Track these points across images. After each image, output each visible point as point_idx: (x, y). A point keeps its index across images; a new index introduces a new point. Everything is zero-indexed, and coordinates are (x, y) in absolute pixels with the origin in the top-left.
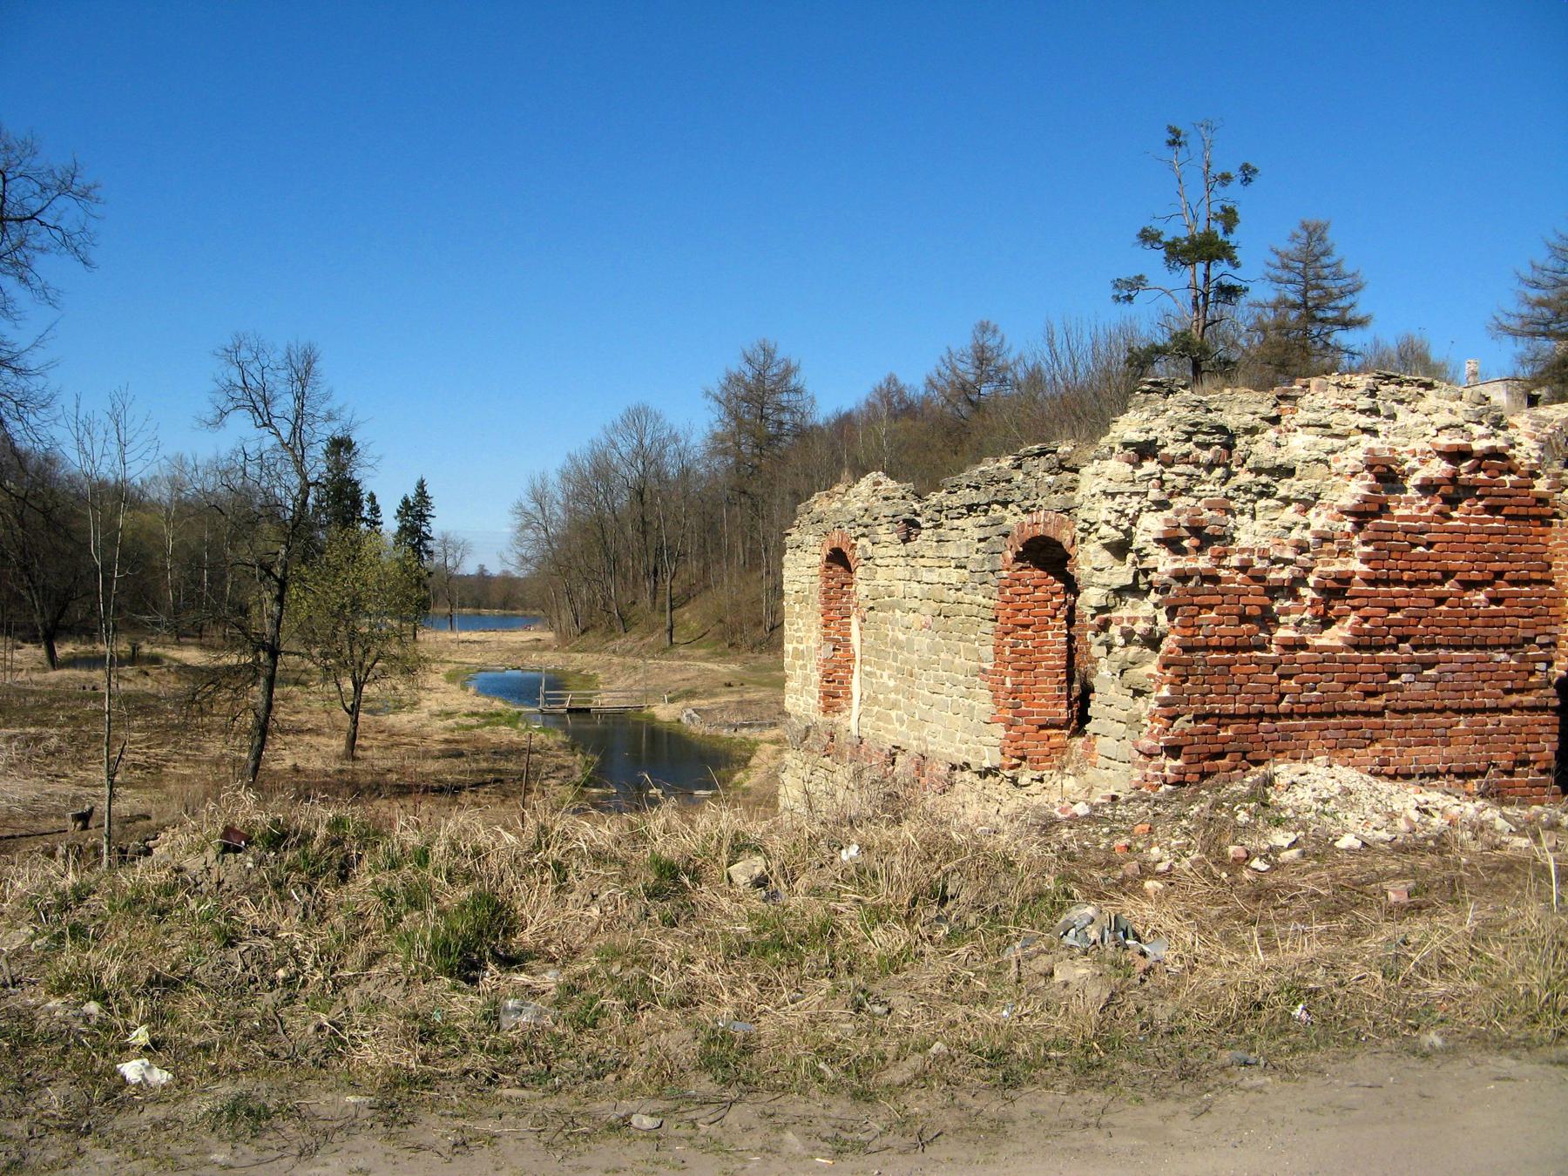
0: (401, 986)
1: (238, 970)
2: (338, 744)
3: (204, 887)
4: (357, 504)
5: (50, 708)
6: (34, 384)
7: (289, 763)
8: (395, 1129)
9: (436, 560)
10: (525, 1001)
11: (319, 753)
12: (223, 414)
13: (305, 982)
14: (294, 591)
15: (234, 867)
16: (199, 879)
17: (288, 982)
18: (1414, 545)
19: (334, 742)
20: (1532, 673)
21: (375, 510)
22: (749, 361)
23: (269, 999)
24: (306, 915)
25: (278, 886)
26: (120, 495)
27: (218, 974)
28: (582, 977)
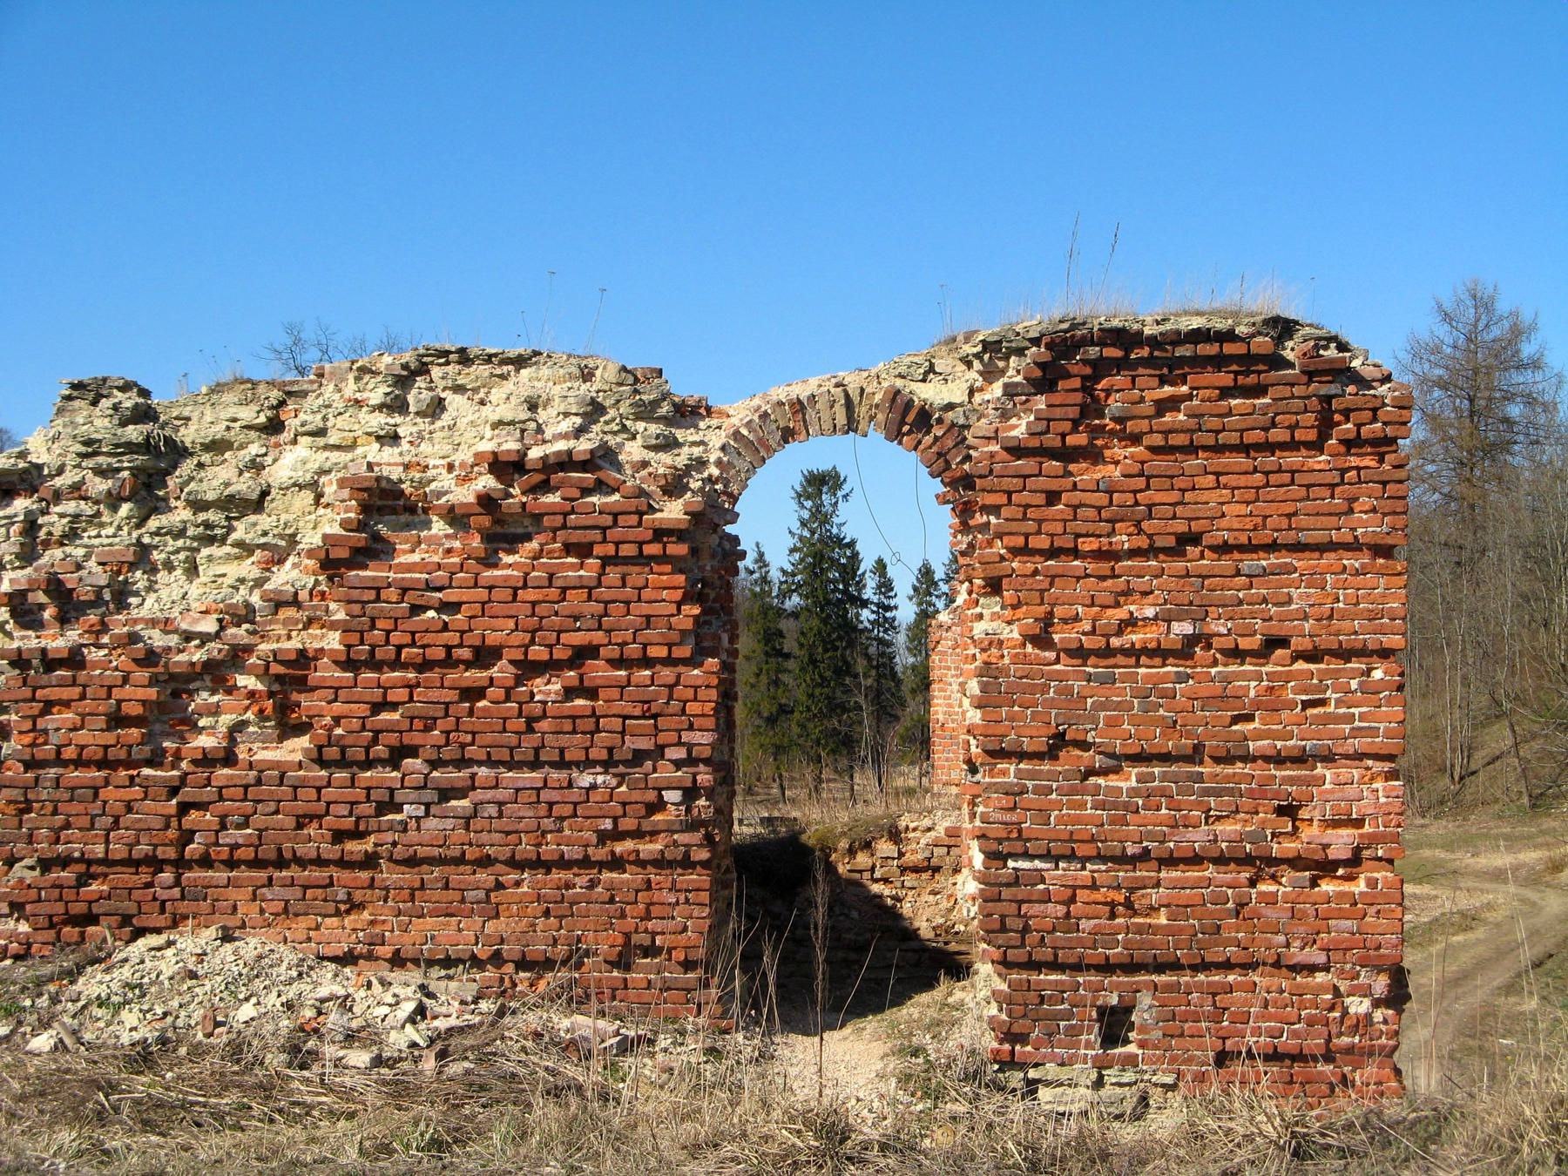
4: (850, 569)
18: (416, 609)
20: (660, 805)
21: (886, 586)
22: (1447, 318)
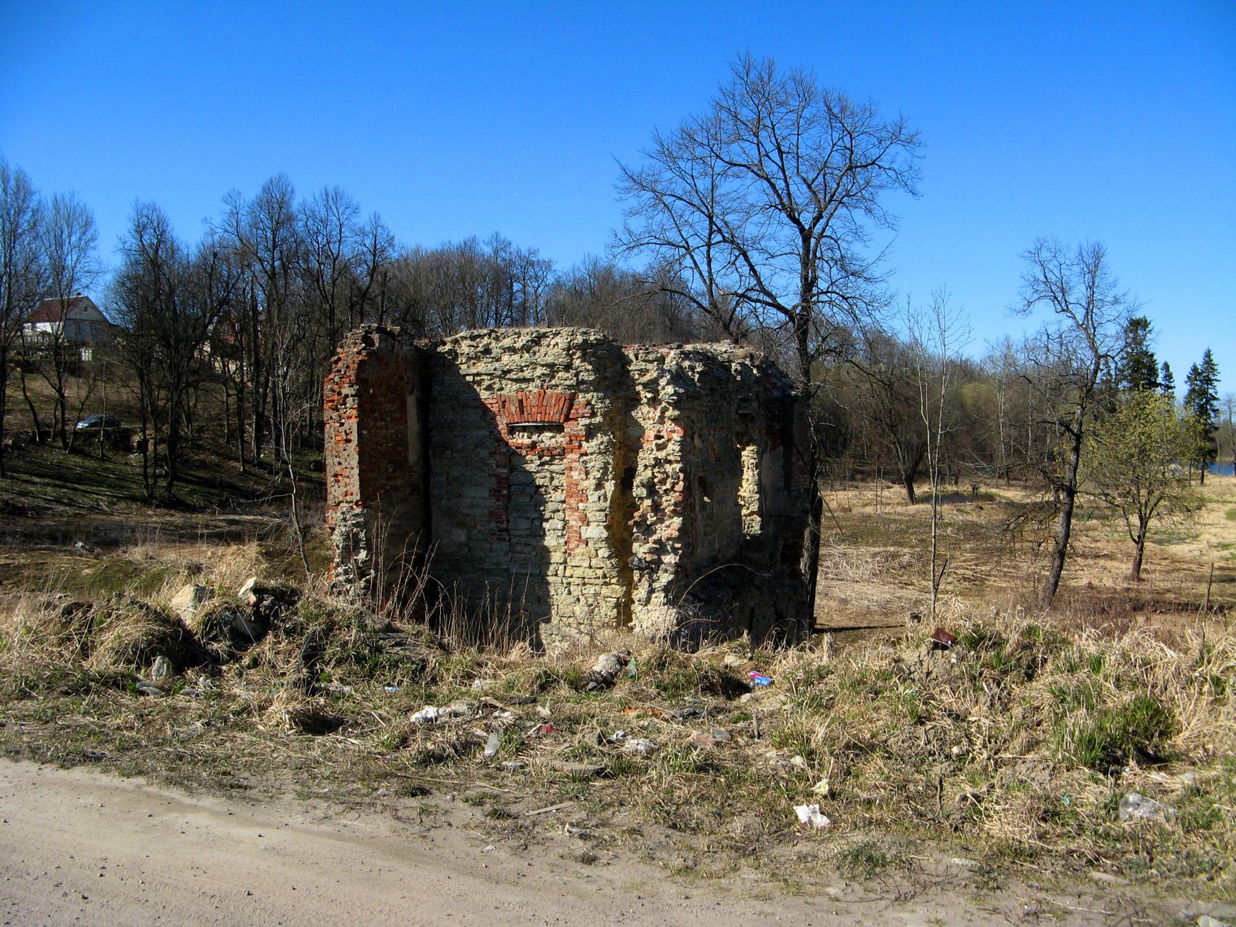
0: (1047, 771)
1: (922, 744)
2: (1127, 567)
3: (916, 676)
4: (1152, 370)
5: (906, 532)
6: (878, 289)
7: (1084, 582)
8: (985, 891)
9: (1222, 417)
10: (1145, 798)
11: (1110, 575)
12: (1029, 303)
13: (973, 759)
14: (1090, 442)
15: (941, 661)
16: (912, 669)
17: (961, 757)
19: (1124, 566)
21: (1169, 377)
23: (938, 769)
24: (992, 705)
25: (973, 679)
26: (964, 371)
27: (906, 745)
28: (1208, 782)
